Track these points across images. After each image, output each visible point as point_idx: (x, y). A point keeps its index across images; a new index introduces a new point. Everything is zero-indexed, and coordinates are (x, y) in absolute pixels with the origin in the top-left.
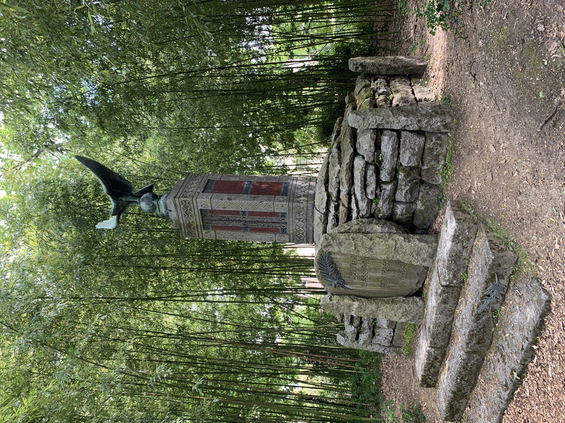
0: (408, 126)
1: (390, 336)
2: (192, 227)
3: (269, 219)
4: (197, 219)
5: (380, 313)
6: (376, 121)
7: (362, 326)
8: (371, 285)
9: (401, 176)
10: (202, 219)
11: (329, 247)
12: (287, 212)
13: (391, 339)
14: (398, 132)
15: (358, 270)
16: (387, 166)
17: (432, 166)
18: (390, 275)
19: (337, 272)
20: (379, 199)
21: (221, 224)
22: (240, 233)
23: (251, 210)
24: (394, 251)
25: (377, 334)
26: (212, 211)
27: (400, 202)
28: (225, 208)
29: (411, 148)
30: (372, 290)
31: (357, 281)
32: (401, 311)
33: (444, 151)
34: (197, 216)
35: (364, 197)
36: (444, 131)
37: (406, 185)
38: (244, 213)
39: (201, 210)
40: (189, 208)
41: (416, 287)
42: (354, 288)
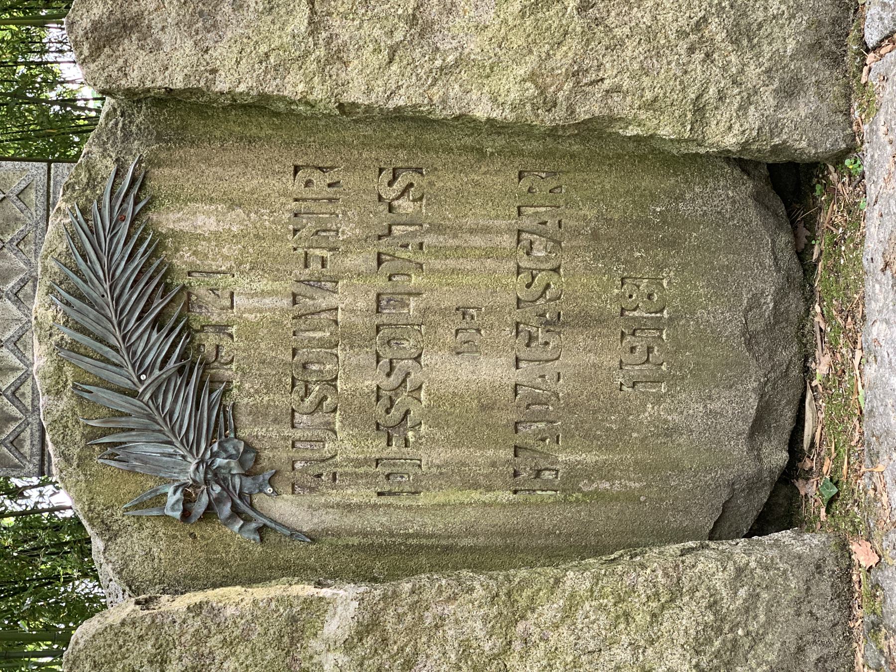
11: (129, 45)
15: (350, 338)
30: (456, 521)
41: (750, 470)
42: (330, 519)
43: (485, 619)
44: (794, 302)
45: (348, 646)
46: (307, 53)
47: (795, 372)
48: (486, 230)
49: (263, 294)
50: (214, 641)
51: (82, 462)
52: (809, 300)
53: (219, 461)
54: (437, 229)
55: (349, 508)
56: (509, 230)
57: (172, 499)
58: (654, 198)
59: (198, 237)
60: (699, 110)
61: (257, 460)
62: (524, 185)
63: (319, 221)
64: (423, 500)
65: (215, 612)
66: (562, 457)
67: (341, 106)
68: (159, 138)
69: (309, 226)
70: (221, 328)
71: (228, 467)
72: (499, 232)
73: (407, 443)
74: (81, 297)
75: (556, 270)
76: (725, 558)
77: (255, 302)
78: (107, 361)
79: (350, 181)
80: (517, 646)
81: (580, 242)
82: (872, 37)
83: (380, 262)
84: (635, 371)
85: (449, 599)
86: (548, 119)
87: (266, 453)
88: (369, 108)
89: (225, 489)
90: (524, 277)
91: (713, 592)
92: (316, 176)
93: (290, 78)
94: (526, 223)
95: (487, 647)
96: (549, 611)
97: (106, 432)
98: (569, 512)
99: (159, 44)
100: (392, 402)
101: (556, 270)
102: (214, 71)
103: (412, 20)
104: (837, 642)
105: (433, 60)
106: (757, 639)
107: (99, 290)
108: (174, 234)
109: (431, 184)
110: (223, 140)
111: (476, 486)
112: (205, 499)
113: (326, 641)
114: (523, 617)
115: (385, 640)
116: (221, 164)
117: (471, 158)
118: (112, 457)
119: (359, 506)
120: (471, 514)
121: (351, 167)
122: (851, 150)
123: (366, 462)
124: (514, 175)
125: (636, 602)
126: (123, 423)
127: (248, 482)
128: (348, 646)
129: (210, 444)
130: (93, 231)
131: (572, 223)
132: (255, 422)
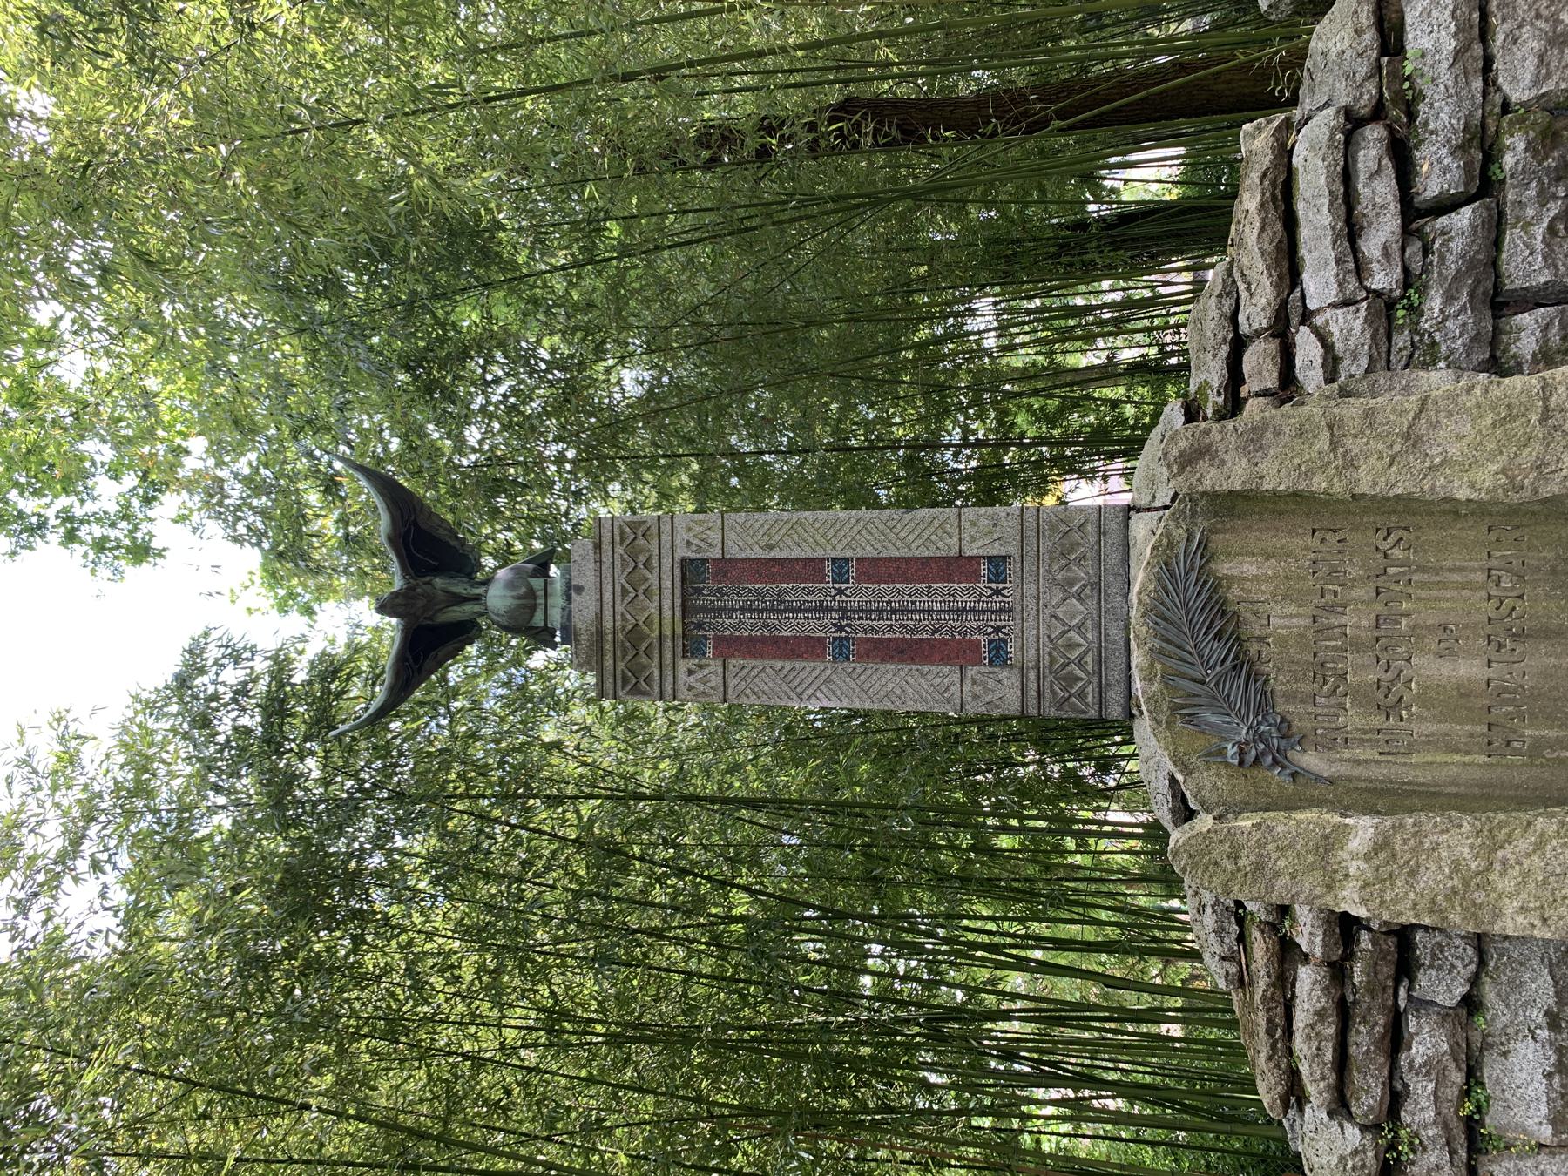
2: (644, 645)
3: (935, 595)
4: (667, 606)
5: (1508, 884)
7: (1405, 1116)
8: (1431, 742)
9: (1515, 151)
11: (1203, 464)
12: (1013, 550)
15: (1356, 645)
19: (1244, 666)
20: (1423, 291)
21: (750, 626)
22: (819, 666)
23: (870, 552)
24: (1540, 432)
26: (725, 567)
27: (1531, 300)
28: (771, 547)
30: (1441, 775)
31: (1353, 718)
34: (667, 593)
35: (1353, 282)
37: (1544, 198)
38: (841, 651)
40: (642, 559)
42: (1344, 769)
43: (1472, 847)
45: (1367, 858)
46: (1329, 463)
48: (1462, 569)
49: (1292, 616)
50: (1270, 847)
51: (1169, 725)
53: (1263, 728)
54: (1422, 569)
55: (1358, 762)
56: (1481, 569)
57: (1231, 752)
59: (1244, 579)
61: (1289, 727)
62: (1493, 536)
63: (1332, 566)
64: (1414, 759)
66: (1528, 732)
67: (1353, 496)
68: (1216, 516)
69: (1324, 570)
70: (1261, 639)
71: (1269, 732)
72: (1473, 570)
73: (1401, 719)
74: (1165, 619)
75: (1521, 597)
77: (1285, 622)
78: (1184, 660)
79: (1354, 538)
80: (1497, 866)
81: (1540, 576)
83: (1378, 593)
85: (1442, 832)
87: (1296, 723)
88: (1374, 496)
89: (1267, 746)
92: (1328, 537)
93: (1316, 479)
94: (1495, 563)
95: (1473, 865)
96: (1523, 844)
97: (1184, 707)
98: (1535, 772)
99: (1223, 462)
100: (1389, 690)
101: (1521, 597)
102: (1262, 477)
103: (1407, 436)
105: (1423, 462)
108: (1227, 577)
109: (1417, 538)
110: (1261, 514)
111: (1457, 751)
112: (1253, 752)
113: (1351, 853)
114: (1502, 847)
115: (1394, 856)
116: (1260, 530)
117: (1449, 518)
118: (1189, 722)
119: (1366, 761)
120: (1454, 770)
121: (1355, 528)
123: (1370, 731)
124: (1484, 529)
126: (1196, 701)
127: (1283, 742)
128: (1367, 858)
129: (1256, 716)
130: (1173, 576)
131: (1533, 562)
132: (1287, 702)
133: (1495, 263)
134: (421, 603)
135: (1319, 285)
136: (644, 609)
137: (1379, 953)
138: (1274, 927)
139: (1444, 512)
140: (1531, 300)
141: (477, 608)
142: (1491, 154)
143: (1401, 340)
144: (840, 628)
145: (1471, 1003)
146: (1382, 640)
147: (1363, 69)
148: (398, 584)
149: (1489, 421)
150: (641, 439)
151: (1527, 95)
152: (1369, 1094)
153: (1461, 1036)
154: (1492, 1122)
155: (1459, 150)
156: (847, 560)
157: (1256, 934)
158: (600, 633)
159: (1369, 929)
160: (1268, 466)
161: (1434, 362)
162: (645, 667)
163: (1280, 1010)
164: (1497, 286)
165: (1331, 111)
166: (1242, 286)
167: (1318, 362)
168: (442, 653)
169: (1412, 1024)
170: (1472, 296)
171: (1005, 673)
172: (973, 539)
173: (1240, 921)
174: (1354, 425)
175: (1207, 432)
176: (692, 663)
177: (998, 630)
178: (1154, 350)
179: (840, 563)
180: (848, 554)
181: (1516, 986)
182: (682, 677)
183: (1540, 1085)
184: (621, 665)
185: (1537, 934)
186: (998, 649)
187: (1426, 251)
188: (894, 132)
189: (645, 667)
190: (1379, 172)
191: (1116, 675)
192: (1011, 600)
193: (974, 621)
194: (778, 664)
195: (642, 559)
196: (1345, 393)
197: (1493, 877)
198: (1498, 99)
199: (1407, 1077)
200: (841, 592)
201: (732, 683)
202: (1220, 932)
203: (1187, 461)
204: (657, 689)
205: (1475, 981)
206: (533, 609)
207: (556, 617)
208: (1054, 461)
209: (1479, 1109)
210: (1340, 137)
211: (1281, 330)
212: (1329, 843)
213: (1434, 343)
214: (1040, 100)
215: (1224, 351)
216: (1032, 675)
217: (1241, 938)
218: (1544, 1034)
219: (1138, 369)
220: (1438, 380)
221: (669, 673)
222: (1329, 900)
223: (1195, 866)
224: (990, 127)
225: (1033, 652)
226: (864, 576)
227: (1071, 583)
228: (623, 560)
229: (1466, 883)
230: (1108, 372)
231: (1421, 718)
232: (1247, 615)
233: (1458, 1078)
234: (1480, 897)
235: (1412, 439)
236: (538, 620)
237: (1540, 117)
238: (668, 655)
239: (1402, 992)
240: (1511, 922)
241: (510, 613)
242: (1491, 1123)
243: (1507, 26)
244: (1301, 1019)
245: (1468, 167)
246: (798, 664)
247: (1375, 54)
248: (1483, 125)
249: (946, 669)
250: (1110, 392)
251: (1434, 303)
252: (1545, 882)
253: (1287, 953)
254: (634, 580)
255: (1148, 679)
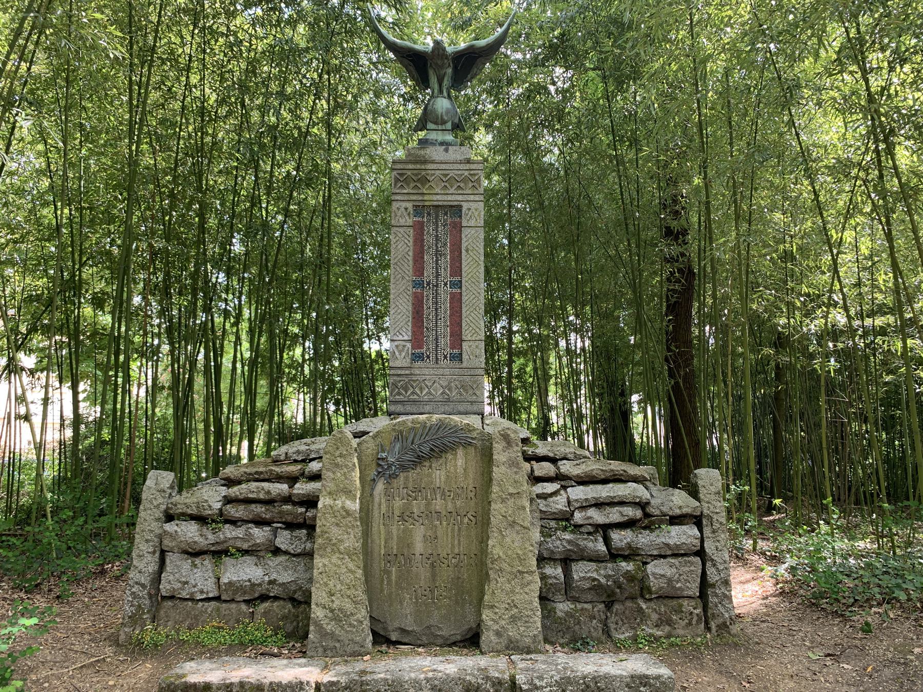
0: (714, 565)
1: (192, 594)
2: (419, 185)
3: (444, 329)
4: (438, 197)
5: (334, 559)
6: (717, 513)
8: (389, 534)
9: (626, 566)
10: (452, 206)
11: (504, 444)
12: (464, 365)
13: (184, 594)
14: (701, 553)
15: (428, 504)
16: (644, 539)
17: (649, 617)
18: (422, 572)
19: (419, 460)
20: (572, 532)
21: (429, 239)
23: (464, 299)
25: (198, 561)
26: (457, 228)
27: (567, 573)
28: (467, 251)
29: (680, 575)
30: (376, 537)
31: (398, 503)
32: (348, 606)
33: (681, 632)
34: (445, 198)
35: (577, 505)
36: (713, 625)
38: (418, 284)
39: (459, 208)
41: (390, 628)
42: (377, 500)
44: (440, 641)
45: (343, 507)
47: (419, 642)
48: (459, 544)
50: (345, 470)
51: (394, 430)
52: (441, 646)
54: (459, 529)
55: (380, 505)
58: (470, 596)
60: (492, 607)
62: (473, 556)
64: (382, 527)
65: (353, 470)
70: (430, 467)
76: (365, 618)
79: (472, 503)
82: (512, 657)
84: (419, 591)
86: (489, 562)
90: (446, 556)
91: (356, 614)
94: (462, 556)
96: (351, 565)
103: (514, 522)
104: (341, 652)
106: (342, 627)
107: (440, 434)
121: (476, 504)
122: (482, 653)
125: (353, 591)
128: (343, 507)
133: (583, 559)
134: (439, 62)
135: (578, 493)
136: (437, 185)
137: (297, 516)
138: (303, 474)
139: (482, 538)
140: (567, 573)
141: (436, 91)
142: (626, 558)
143: (553, 524)
144: (428, 284)
145: (277, 551)
146: (430, 514)
147: (664, 509)
148: (450, 49)
149: (519, 552)
150: (519, 160)
151: (649, 571)
152: (235, 511)
153: (262, 548)
154: (226, 559)
155: (629, 546)
156: (461, 287)
157: (299, 467)
158: (425, 162)
159: (306, 512)
160: (503, 469)
161: (543, 536)
162: (408, 185)
163: (267, 477)
164: (573, 560)
165: (649, 496)
166: (578, 462)
167: (545, 491)
168: (412, 68)
169: (268, 529)
170: (569, 550)
171: (409, 360)
172: (470, 347)
173: (303, 461)
174: (519, 502)
175: (517, 445)
176: (411, 209)
177: (428, 357)
178: (555, 429)
179: (459, 284)
180: (464, 288)
181: (286, 568)
182: (404, 204)
183: (245, 578)
184: (409, 173)
185: (315, 571)
186: (420, 357)
187: (589, 533)
188: (674, 300)
189: (408, 185)
190: (623, 515)
191: (408, 408)
192: (442, 363)
193: (432, 346)
194: (411, 253)
195: (462, 185)
196: (532, 500)
197: (337, 555)
198: (649, 560)
199: (244, 527)
200: (446, 284)
201: (401, 230)
202: (298, 452)
203: (505, 437)
204: (398, 191)
205: (286, 553)
206: (436, 123)
207: (433, 136)
208: (499, 378)
209: (232, 555)
210: (638, 500)
211: (559, 477)
212: (349, 493)
213: (551, 536)
214: (686, 373)
215: (551, 455)
216: (407, 372)
217: (296, 461)
218: (266, 578)
219: (547, 421)
220: (536, 535)
221: (406, 198)
222: (324, 493)
223: (336, 440)
224: (674, 349)
225: (418, 372)
226: (453, 296)
227: (449, 390)
228: (462, 175)
229: (334, 545)
230: (545, 407)
231: (399, 530)
232: (441, 461)
233: (245, 546)
234: (329, 550)
235: (513, 524)
236: (430, 126)
237: (640, 575)
238: (414, 198)
239: (280, 525)
240: (318, 561)
241: (434, 111)
242: (225, 559)
243: (677, 563)
244: (266, 485)
245: (622, 549)
246: (411, 263)
247: (670, 514)
248: (638, 555)
249: (410, 334)
250: (534, 410)
251: (568, 536)
252: (336, 573)
253: (292, 480)
254: (451, 181)
255: (413, 422)
